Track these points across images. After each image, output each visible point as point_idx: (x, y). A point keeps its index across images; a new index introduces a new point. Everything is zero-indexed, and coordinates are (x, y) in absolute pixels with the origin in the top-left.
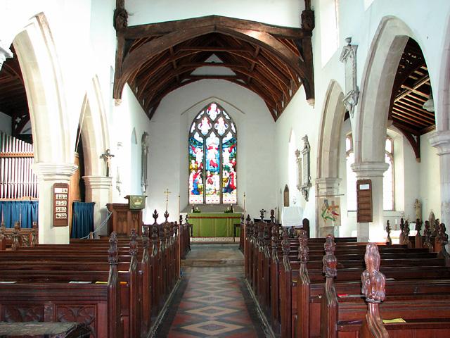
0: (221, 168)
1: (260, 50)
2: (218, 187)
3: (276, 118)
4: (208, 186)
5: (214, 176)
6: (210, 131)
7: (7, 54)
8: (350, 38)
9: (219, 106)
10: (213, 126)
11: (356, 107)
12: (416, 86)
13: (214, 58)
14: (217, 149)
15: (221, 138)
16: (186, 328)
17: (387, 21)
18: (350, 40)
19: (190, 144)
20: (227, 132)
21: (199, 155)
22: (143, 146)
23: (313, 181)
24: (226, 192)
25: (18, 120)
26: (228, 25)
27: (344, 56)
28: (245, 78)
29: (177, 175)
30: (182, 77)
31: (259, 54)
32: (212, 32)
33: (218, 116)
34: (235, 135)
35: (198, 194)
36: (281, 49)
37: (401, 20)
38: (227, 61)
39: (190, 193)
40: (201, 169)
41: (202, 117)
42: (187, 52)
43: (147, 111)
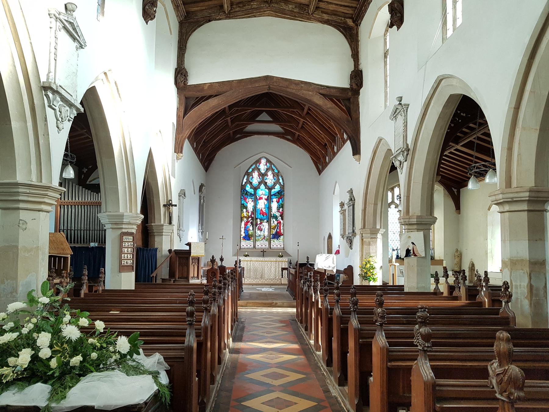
0: (269, 216)
1: (309, 109)
2: (266, 233)
3: (320, 172)
4: (258, 232)
5: (263, 224)
6: (260, 183)
7: (77, 109)
8: (401, 97)
9: (268, 161)
10: (263, 178)
11: (405, 164)
12: (461, 142)
13: (264, 116)
14: (266, 199)
15: (270, 189)
16: (250, 376)
17: (442, 80)
18: (400, 99)
19: (242, 195)
20: (275, 184)
21: (250, 205)
22: (200, 197)
23: (357, 231)
24: (274, 238)
25: (85, 170)
26: (281, 85)
27: (395, 114)
28: (293, 135)
29: (231, 222)
30: (235, 133)
31: (308, 113)
32: (267, 91)
33: (267, 170)
34: (282, 187)
35: (249, 239)
36: (330, 108)
37: (459, 79)
38: (276, 119)
39: (242, 239)
40: (252, 217)
41: (253, 170)
42: (241, 111)
43: (203, 165)
